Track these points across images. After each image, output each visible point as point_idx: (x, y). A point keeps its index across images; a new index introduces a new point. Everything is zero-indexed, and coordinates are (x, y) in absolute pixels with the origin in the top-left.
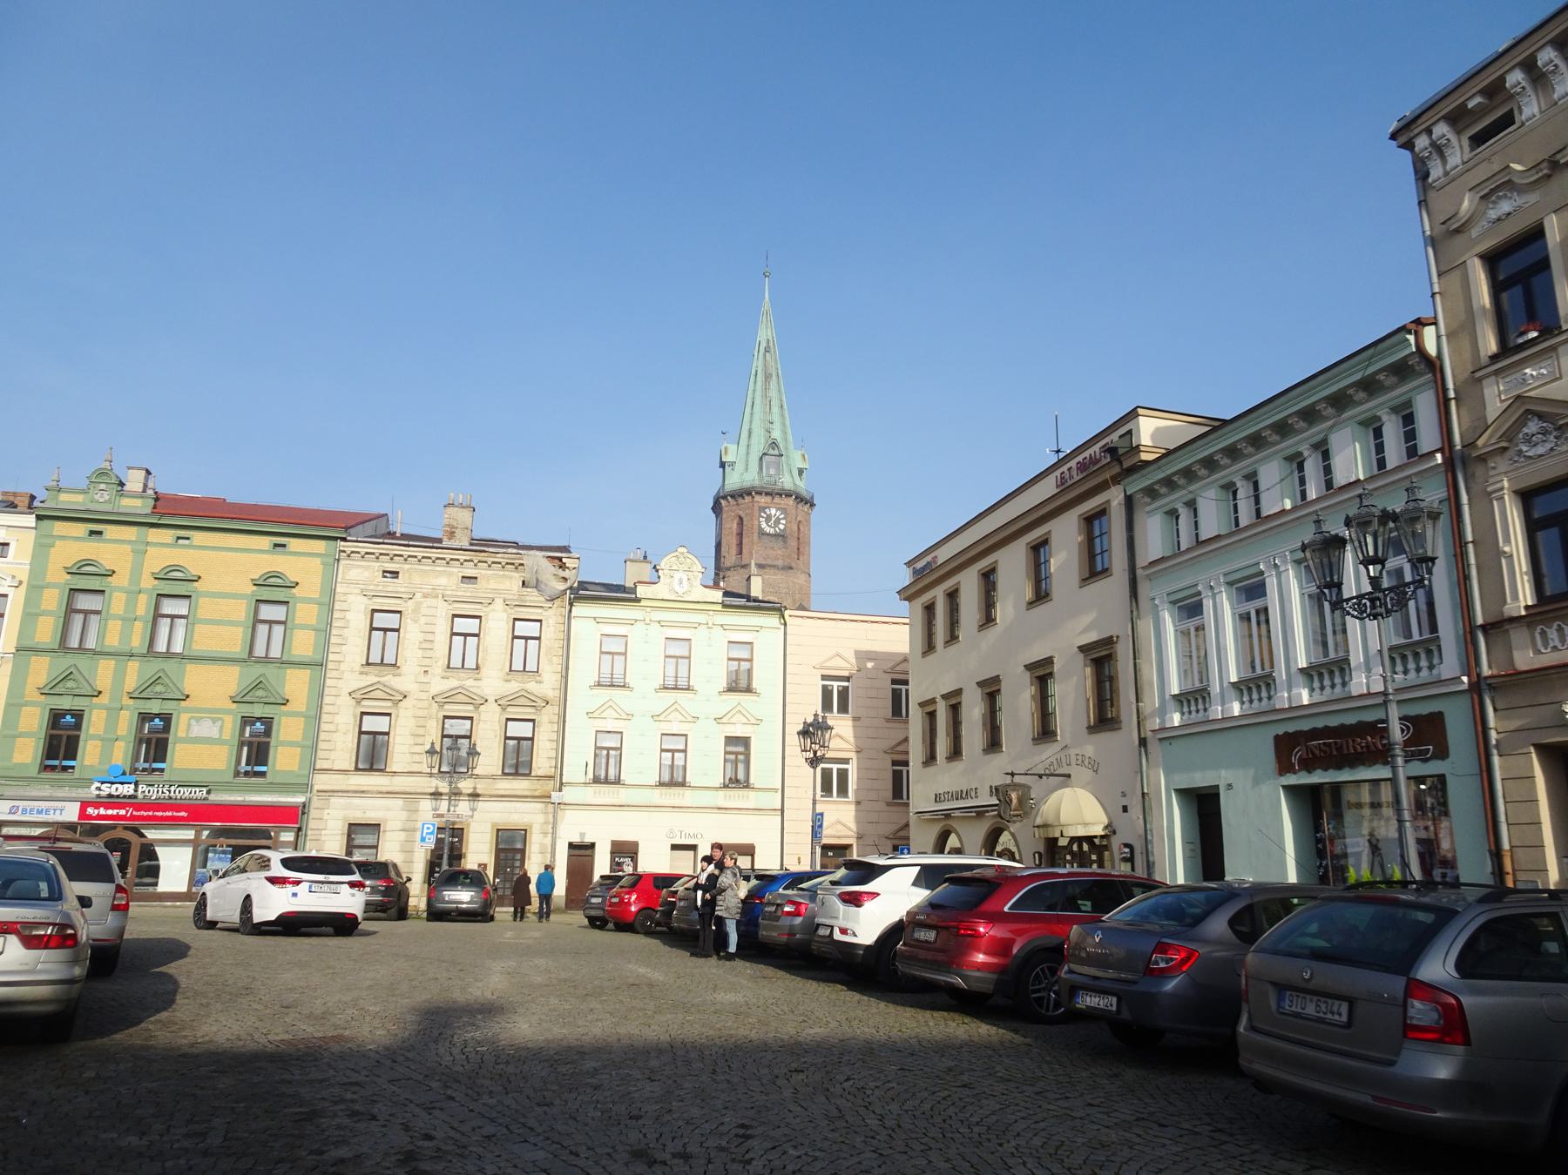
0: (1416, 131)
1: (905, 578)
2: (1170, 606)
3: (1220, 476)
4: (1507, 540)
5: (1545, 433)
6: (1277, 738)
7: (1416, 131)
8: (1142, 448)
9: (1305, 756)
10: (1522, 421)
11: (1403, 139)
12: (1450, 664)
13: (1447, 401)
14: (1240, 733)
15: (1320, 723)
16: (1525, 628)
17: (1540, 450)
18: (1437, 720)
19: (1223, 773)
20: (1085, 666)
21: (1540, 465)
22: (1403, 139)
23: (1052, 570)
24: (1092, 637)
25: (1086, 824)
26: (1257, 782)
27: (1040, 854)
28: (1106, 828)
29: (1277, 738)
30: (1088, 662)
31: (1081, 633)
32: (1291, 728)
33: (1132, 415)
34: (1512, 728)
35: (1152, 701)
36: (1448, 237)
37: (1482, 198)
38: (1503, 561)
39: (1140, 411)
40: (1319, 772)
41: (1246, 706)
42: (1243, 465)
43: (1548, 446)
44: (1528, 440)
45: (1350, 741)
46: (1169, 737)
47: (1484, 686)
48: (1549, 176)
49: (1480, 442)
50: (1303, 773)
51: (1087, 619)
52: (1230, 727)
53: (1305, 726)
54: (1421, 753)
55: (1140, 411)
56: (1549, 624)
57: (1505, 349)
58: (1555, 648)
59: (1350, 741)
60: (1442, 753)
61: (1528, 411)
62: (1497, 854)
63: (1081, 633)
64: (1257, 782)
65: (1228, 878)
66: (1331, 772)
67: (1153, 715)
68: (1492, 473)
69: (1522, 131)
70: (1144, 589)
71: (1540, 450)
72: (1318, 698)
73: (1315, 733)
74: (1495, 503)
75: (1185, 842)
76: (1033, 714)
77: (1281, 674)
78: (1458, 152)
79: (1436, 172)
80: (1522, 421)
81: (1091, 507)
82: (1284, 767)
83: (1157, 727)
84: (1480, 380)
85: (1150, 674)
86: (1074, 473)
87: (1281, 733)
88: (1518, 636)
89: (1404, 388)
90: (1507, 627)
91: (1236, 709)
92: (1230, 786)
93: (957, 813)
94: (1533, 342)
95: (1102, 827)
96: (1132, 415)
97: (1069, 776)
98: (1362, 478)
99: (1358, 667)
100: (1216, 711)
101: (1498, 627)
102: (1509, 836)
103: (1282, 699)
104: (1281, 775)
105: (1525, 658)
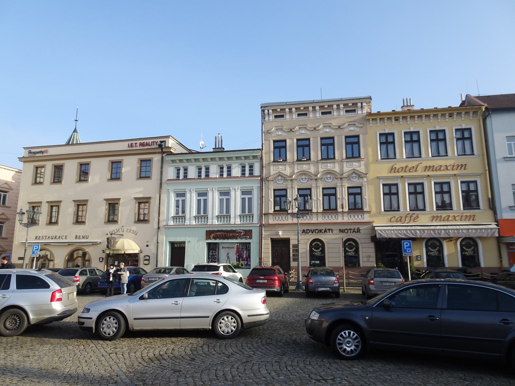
0: (266, 109)
1: (24, 153)
2: (174, 193)
3: (198, 164)
4: (366, 195)
5: (330, 178)
6: (207, 231)
7: (266, 109)
8: (172, 148)
9: (215, 236)
10: (352, 174)
11: (263, 109)
12: (256, 220)
13: (263, 167)
14: (203, 228)
15: (220, 229)
16: (347, 214)
17: (329, 181)
18: (251, 231)
19: (187, 238)
20: (136, 203)
21: (280, 185)
22: (263, 109)
23: (123, 172)
24: (141, 196)
25: (133, 250)
26: (198, 241)
27: (103, 258)
28: (139, 251)
29: (207, 231)
30: (137, 203)
31: (135, 193)
32: (211, 229)
33: (168, 137)
34: (267, 234)
35: (163, 217)
36: (266, 133)
37: (349, 124)
38: (344, 200)
39: (170, 137)
40: (226, 240)
41: (175, 223)
42: (206, 163)
43: (331, 181)
44: (278, 180)
45: (229, 234)
46: (167, 227)
47: (263, 226)
48: (337, 129)
49: (270, 178)
50: (214, 240)
51: (142, 189)
52: (191, 227)
53: (216, 229)
54: (246, 238)
55: (170, 137)
56: (280, 215)
57: (274, 161)
58: (284, 220)
59: (229, 234)
60: (251, 238)
61: (280, 175)
62: (260, 259)
63: (135, 193)
64: (198, 241)
65: (327, 265)
66: (221, 240)
67: (163, 221)
68: (343, 182)
69: (285, 120)
70: (164, 186)
71: (329, 181)
72: (219, 223)
73: (218, 231)
74: (343, 188)
75: (169, 255)
76: (106, 215)
77: (210, 216)
78: (272, 118)
79: (267, 118)
80: (352, 174)
81: (62, 163)
82: (208, 237)
83: (165, 224)
84: (318, 163)
85: (164, 209)
86: (138, 145)
87: (208, 230)
88: (271, 217)
89: (180, 164)
90: (269, 215)
91: (194, 223)
92: (189, 242)
93: (52, 244)
94: (304, 161)
95: (138, 250)
96: (168, 137)
97: (123, 235)
98: (218, 177)
99: (232, 218)
100: (187, 222)
101: (267, 214)
102: (458, 255)
103: (210, 222)
104: (206, 240)
105: (271, 222)
